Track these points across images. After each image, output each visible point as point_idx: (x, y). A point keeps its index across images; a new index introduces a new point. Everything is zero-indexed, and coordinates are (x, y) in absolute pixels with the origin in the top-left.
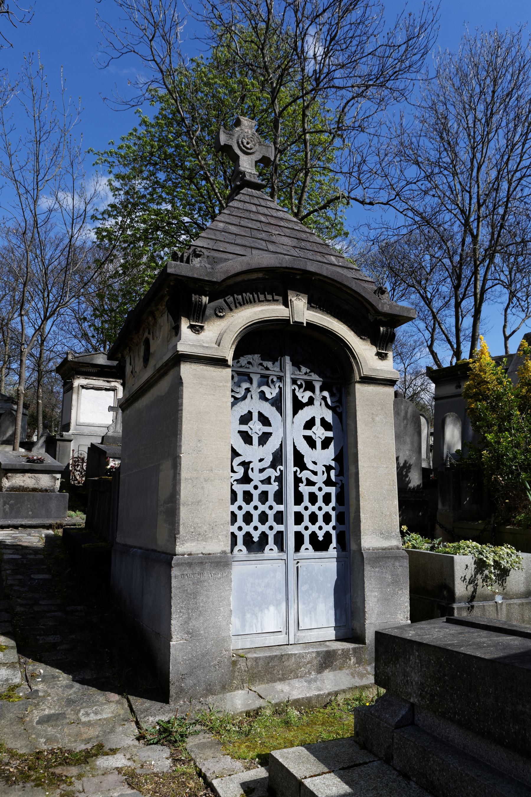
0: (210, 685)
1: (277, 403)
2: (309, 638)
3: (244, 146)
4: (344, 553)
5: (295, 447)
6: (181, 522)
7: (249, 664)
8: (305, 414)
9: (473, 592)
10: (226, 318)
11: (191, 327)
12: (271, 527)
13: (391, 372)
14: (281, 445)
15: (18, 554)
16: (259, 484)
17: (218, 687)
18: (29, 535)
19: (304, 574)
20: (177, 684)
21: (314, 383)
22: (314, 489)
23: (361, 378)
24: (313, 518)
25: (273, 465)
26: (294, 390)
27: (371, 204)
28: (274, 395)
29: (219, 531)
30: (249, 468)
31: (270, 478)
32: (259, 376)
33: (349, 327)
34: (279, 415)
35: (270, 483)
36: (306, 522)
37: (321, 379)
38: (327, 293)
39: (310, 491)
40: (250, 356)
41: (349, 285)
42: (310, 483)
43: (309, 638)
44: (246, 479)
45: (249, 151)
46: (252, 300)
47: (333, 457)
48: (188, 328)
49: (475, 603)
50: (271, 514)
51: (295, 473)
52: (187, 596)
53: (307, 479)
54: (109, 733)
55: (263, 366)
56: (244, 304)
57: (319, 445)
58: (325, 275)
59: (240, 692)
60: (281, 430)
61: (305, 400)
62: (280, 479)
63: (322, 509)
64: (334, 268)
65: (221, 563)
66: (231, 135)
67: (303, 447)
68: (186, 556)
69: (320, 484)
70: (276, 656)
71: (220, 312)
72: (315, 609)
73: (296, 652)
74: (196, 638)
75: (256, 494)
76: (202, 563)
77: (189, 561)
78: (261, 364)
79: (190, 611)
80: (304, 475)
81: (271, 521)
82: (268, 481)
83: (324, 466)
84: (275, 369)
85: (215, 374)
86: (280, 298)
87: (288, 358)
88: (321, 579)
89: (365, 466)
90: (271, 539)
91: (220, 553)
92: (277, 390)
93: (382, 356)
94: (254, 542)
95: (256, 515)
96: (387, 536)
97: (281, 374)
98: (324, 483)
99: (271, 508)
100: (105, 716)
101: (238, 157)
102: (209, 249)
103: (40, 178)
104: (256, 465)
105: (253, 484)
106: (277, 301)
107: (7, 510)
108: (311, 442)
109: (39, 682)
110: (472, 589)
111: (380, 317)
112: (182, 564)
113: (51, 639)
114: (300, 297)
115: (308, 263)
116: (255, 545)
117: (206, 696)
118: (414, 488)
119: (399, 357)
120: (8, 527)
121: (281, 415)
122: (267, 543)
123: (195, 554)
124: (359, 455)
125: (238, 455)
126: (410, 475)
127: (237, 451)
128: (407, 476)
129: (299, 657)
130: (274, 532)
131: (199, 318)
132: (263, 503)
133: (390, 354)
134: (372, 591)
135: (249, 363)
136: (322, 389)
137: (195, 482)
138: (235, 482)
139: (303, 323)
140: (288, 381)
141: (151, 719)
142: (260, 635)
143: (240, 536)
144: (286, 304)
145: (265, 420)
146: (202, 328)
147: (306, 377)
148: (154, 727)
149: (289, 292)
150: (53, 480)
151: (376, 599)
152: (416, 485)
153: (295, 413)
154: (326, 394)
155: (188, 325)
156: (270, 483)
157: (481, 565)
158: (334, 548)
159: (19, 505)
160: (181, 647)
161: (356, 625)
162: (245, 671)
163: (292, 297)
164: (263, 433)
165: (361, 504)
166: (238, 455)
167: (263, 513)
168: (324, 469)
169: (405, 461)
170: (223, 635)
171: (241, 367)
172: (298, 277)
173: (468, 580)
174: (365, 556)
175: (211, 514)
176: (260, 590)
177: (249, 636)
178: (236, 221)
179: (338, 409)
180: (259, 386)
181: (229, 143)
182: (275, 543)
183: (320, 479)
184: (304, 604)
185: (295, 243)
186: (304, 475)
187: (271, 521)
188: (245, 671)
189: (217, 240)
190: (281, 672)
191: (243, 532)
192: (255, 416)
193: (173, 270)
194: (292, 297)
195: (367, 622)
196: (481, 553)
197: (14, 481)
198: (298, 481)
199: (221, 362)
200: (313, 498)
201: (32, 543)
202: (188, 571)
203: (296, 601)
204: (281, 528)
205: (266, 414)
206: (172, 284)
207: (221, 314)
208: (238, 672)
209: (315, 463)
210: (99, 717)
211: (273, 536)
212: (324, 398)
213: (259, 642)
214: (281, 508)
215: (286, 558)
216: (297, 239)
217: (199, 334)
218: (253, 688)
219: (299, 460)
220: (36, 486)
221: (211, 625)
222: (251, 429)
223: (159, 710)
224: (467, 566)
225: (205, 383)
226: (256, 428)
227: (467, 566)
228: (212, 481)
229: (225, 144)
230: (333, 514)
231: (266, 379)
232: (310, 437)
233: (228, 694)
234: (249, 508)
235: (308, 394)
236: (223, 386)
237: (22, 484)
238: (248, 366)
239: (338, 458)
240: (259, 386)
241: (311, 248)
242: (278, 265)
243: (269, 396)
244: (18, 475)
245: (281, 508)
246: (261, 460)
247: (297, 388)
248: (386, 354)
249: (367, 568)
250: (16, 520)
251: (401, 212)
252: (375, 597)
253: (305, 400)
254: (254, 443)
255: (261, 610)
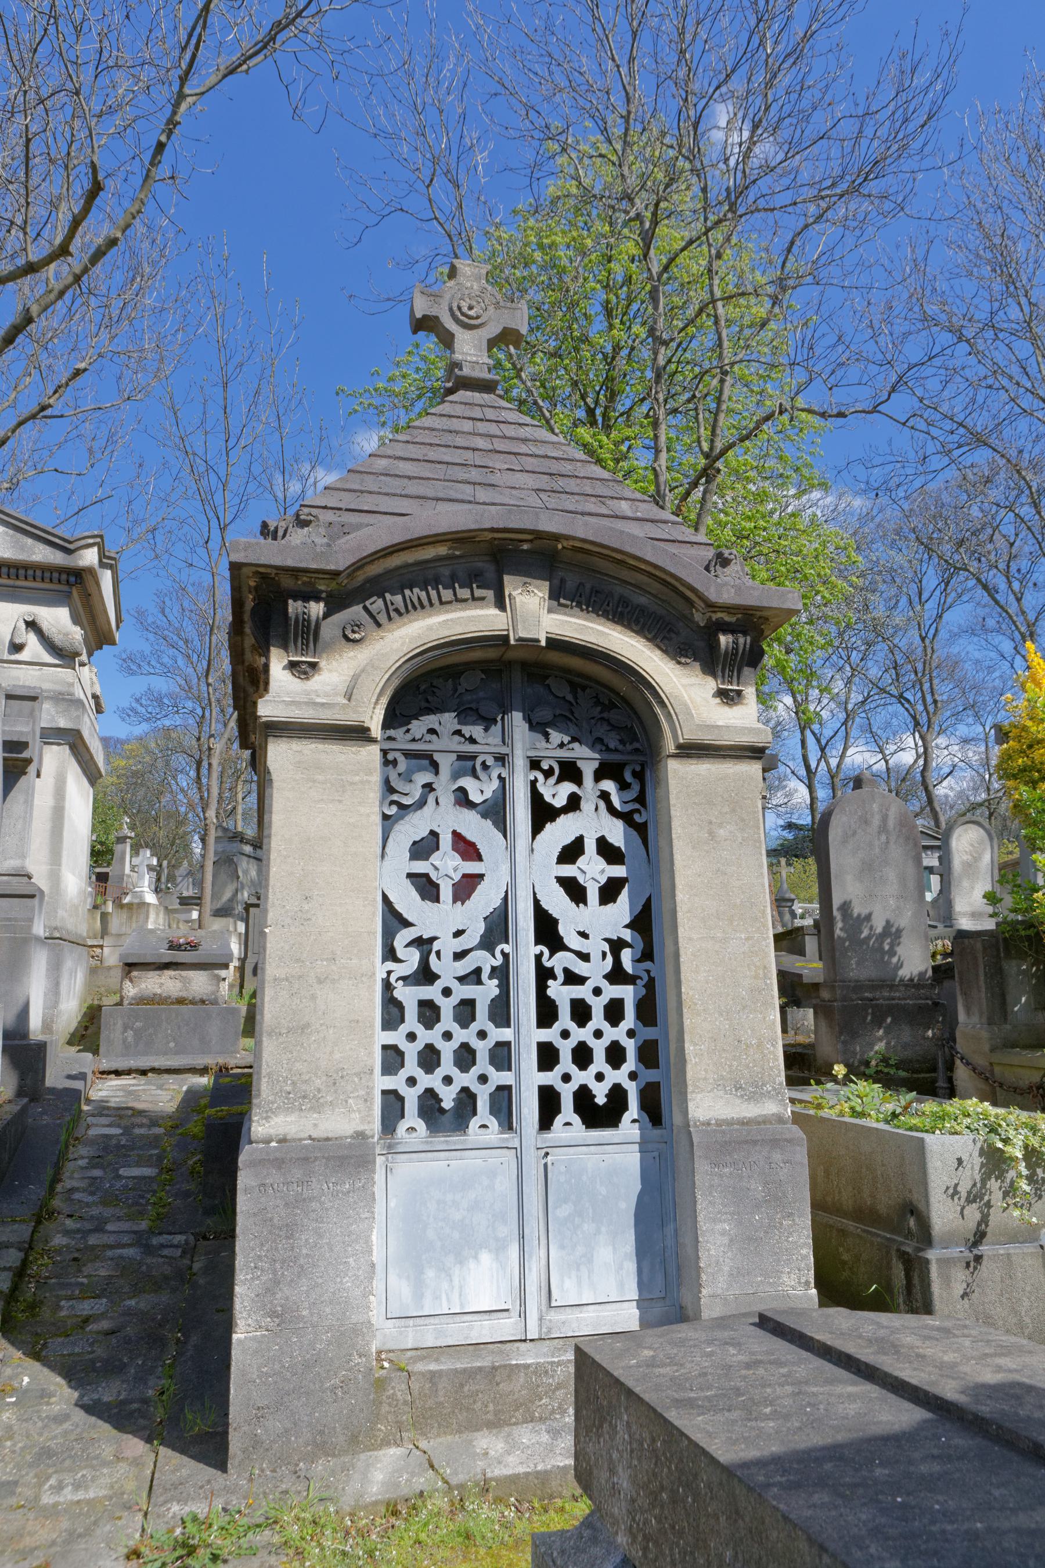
0: (321, 1433)
1: (496, 812)
2: (575, 1325)
3: (463, 314)
4: (657, 1132)
5: (537, 902)
6: (264, 1072)
7: (415, 1386)
8: (560, 832)
9: (979, 1224)
10: (367, 643)
11: (292, 666)
12: (483, 1079)
13: (751, 730)
14: (505, 899)
15: (119, 1126)
16: (455, 985)
17: (342, 1438)
18: (160, 1087)
19: (562, 1179)
20: (246, 1428)
21: (579, 764)
22: (582, 992)
23: (679, 747)
24: (582, 1056)
25: (488, 943)
26: (534, 783)
27: (841, 415)
28: (488, 794)
29: (349, 1088)
30: (430, 951)
31: (478, 971)
32: (454, 756)
33: (649, 640)
34: (501, 836)
35: (479, 982)
36: (566, 1063)
37: (597, 756)
38: (584, 574)
39: (574, 996)
40: (432, 717)
41: (639, 554)
42: (572, 978)
43: (575, 1325)
44: (425, 975)
45: (472, 322)
46: (426, 602)
47: (627, 920)
48: (284, 668)
49: (984, 1249)
50: (482, 1049)
51: (539, 958)
52: (270, 1232)
53: (566, 971)
54: (80, 1536)
55: (463, 736)
56: (408, 611)
57: (593, 895)
58: (582, 536)
59: (393, 1451)
60: (505, 868)
61: (559, 802)
62: (502, 973)
63: (599, 1034)
64: (620, 525)
65: (350, 1159)
66: (436, 297)
67: (557, 902)
68: (274, 1144)
69: (596, 980)
70: (480, 1369)
71: (353, 632)
72: (588, 1259)
73: (529, 1362)
74: (292, 1326)
75: (447, 1006)
76: (306, 1159)
77: (278, 1155)
78: (458, 732)
79: (278, 1266)
80: (559, 962)
81: (483, 1064)
82: (474, 977)
83: (606, 940)
84: (490, 740)
85: (343, 758)
86: (490, 594)
87: (517, 716)
88: (603, 1191)
89: (695, 936)
90: (483, 1104)
91: (352, 1137)
92: (495, 784)
93: (728, 697)
94: (442, 1111)
95: (447, 1051)
96: (754, 1093)
97: (504, 750)
98: (606, 977)
99: (484, 1035)
100: (91, 1494)
101: (452, 336)
102: (340, 509)
103: (230, 444)
104: (447, 945)
105: (439, 985)
106: (483, 599)
107: (130, 1039)
108: (575, 891)
109: (9, 1404)
110: (978, 1216)
111: (719, 615)
112: (262, 1162)
113: (86, 1307)
114: (531, 588)
115: (542, 516)
116: (446, 1117)
117: (311, 1458)
118: (911, 980)
119: (970, 713)
120: (129, 1072)
121: (505, 837)
122: (474, 1113)
123: (294, 1140)
124: (680, 915)
125: (407, 924)
126: (899, 950)
127: (405, 915)
128: (892, 953)
129: (535, 1373)
130: (490, 1087)
131: (307, 646)
132: (464, 1025)
133: (750, 692)
134: (714, 1221)
135: (432, 731)
136: (599, 776)
137: (296, 986)
138: (401, 982)
139: (538, 641)
140: (520, 763)
141: (175, 1508)
142: (458, 1318)
143: (411, 1097)
144: (500, 603)
145: (467, 849)
146: (314, 666)
147: (564, 754)
148: (171, 1531)
149: (507, 578)
150: (214, 982)
151: (726, 1240)
152: (915, 972)
153: (537, 828)
154: (609, 785)
155: (286, 662)
156: (479, 982)
157: (995, 1161)
158: (634, 1121)
159: (151, 1030)
160: (255, 1345)
161: (687, 1300)
162: (405, 1402)
163: (512, 585)
164: (465, 876)
165: (687, 1022)
166: (407, 924)
167: (465, 1047)
168: (606, 947)
169: (888, 922)
170: (354, 1319)
171: (414, 740)
172: (525, 547)
173: (964, 1195)
174: (696, 1140)
175: (332, 1053)
176: (458, 1216)
177: (432, 1320)
178: (413, 451)
179: (636, 817)
180: (456, 776)
181: (433, 312)
182: (494, 1111)
183: (596, 970)
184: (562, 1247)
185: (544, 482)
186: (559, 962)
187: (483, 1064)
188: (405, 1402)
189: (362, 492)
190: (491, 1407)
191: (419, 1089)
192: (446, 840)
193: (242, 554)
194: (512, 585)
195: (704, 1292)
196: (993, 1130)
197: (143, 986)
198: (544, 975)
199: (358, 734)
200: (581, 1013)
201: (156, 1103)
202: (274, 1177)
203: (543, 1241)
204: (505, 1078)
205: (470, 836)
206: (252, 584)
207: (357, 636)
208: (390, 1405)
209: (584, 935)
210: (80, 1495)
211: (487, 1097)
212: (605, 796)
213: (456, 1333)
214: (506, 1034)
215: (517, 1145)
216: (551, 474)
217: (307, 679)
218: (423, 1444)
219: (547, 930)
220: (184, 994)
221: (326, 1297)
222: (436, 869)
223: (201, 1487)
224: (960, 1161)
225: (320, 778)
226: (447, 866)
227: (960, 1161)
228: (333, 981)
229: (424, 316)
230: (630, 1046)
231: (470, 764)
232: (573, 880)
233: (362, 1456)
234: (432, 1036)
235: (568, 788)
236: (362, 782)
237: (159, 991)
238: (428, 737)
239: (642, 922)
240: (456, 776)
241: (576, 490)
242: (473, 527)
243: (475, 797)
244: (151, 974)
245: (506, 1034)
246: (458, 934)
247: (541, 777)
248: (739, 693)
249: (702, 1168)
250: (145, 1058)
251: (904, 424)
252: (723, 1233)
253: (559, 802)
254: (442, 899)
255: (461, 1262)
